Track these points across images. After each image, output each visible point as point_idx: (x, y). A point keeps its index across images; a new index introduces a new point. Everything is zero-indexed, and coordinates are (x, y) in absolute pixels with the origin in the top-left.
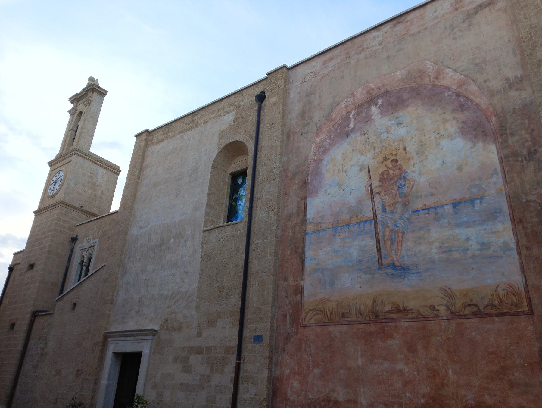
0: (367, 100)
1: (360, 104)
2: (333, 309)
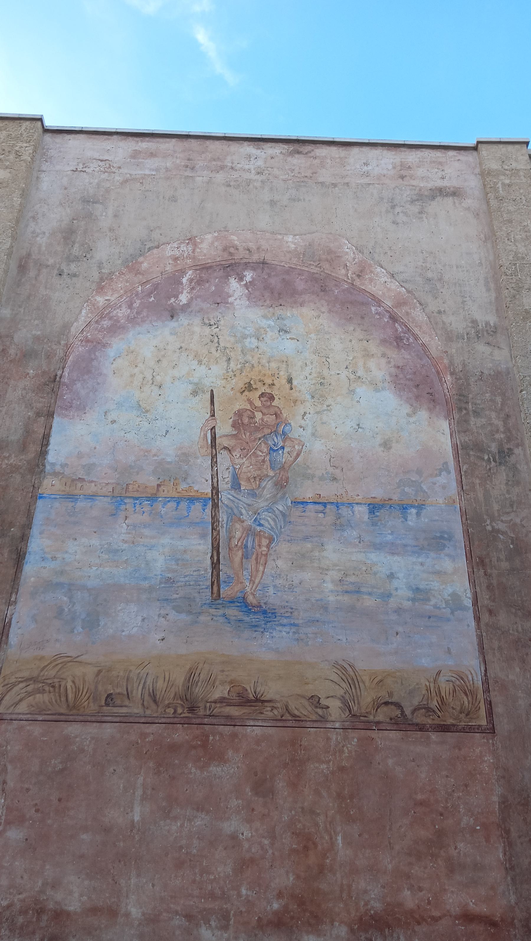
0: (223, 263)
1: (208, 265)
2: (84, 681)
